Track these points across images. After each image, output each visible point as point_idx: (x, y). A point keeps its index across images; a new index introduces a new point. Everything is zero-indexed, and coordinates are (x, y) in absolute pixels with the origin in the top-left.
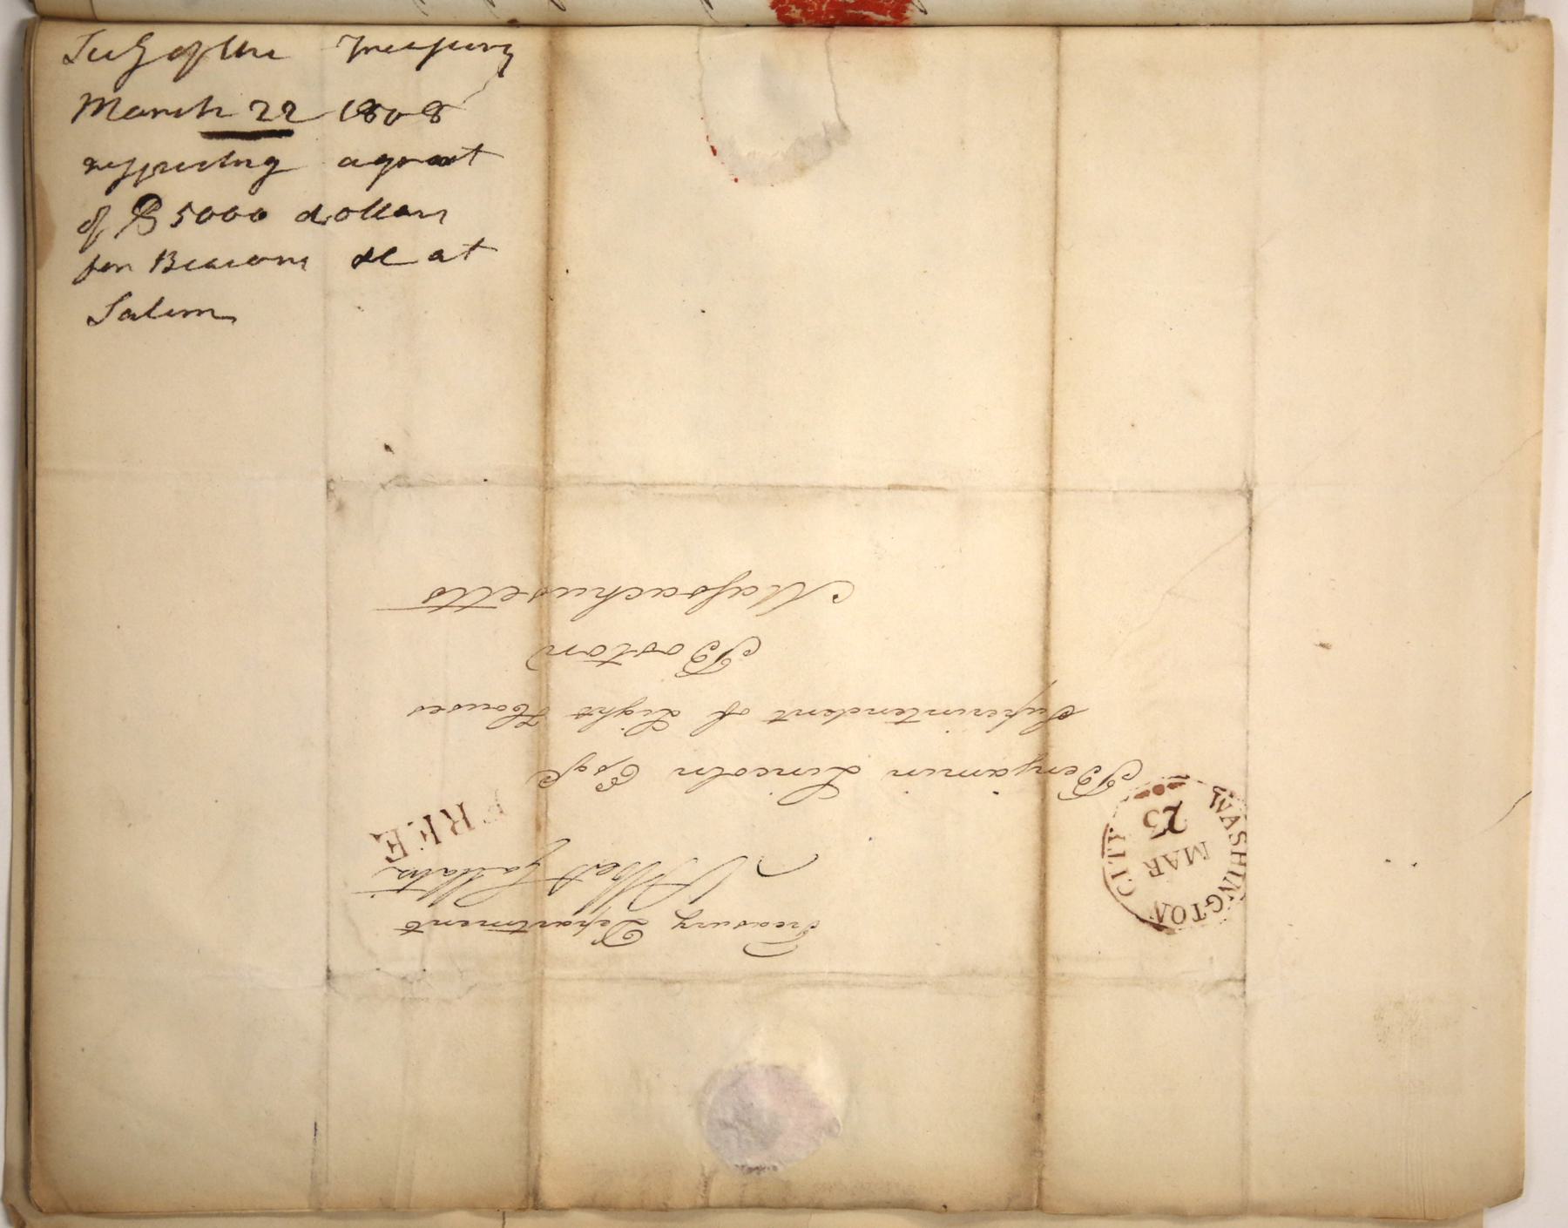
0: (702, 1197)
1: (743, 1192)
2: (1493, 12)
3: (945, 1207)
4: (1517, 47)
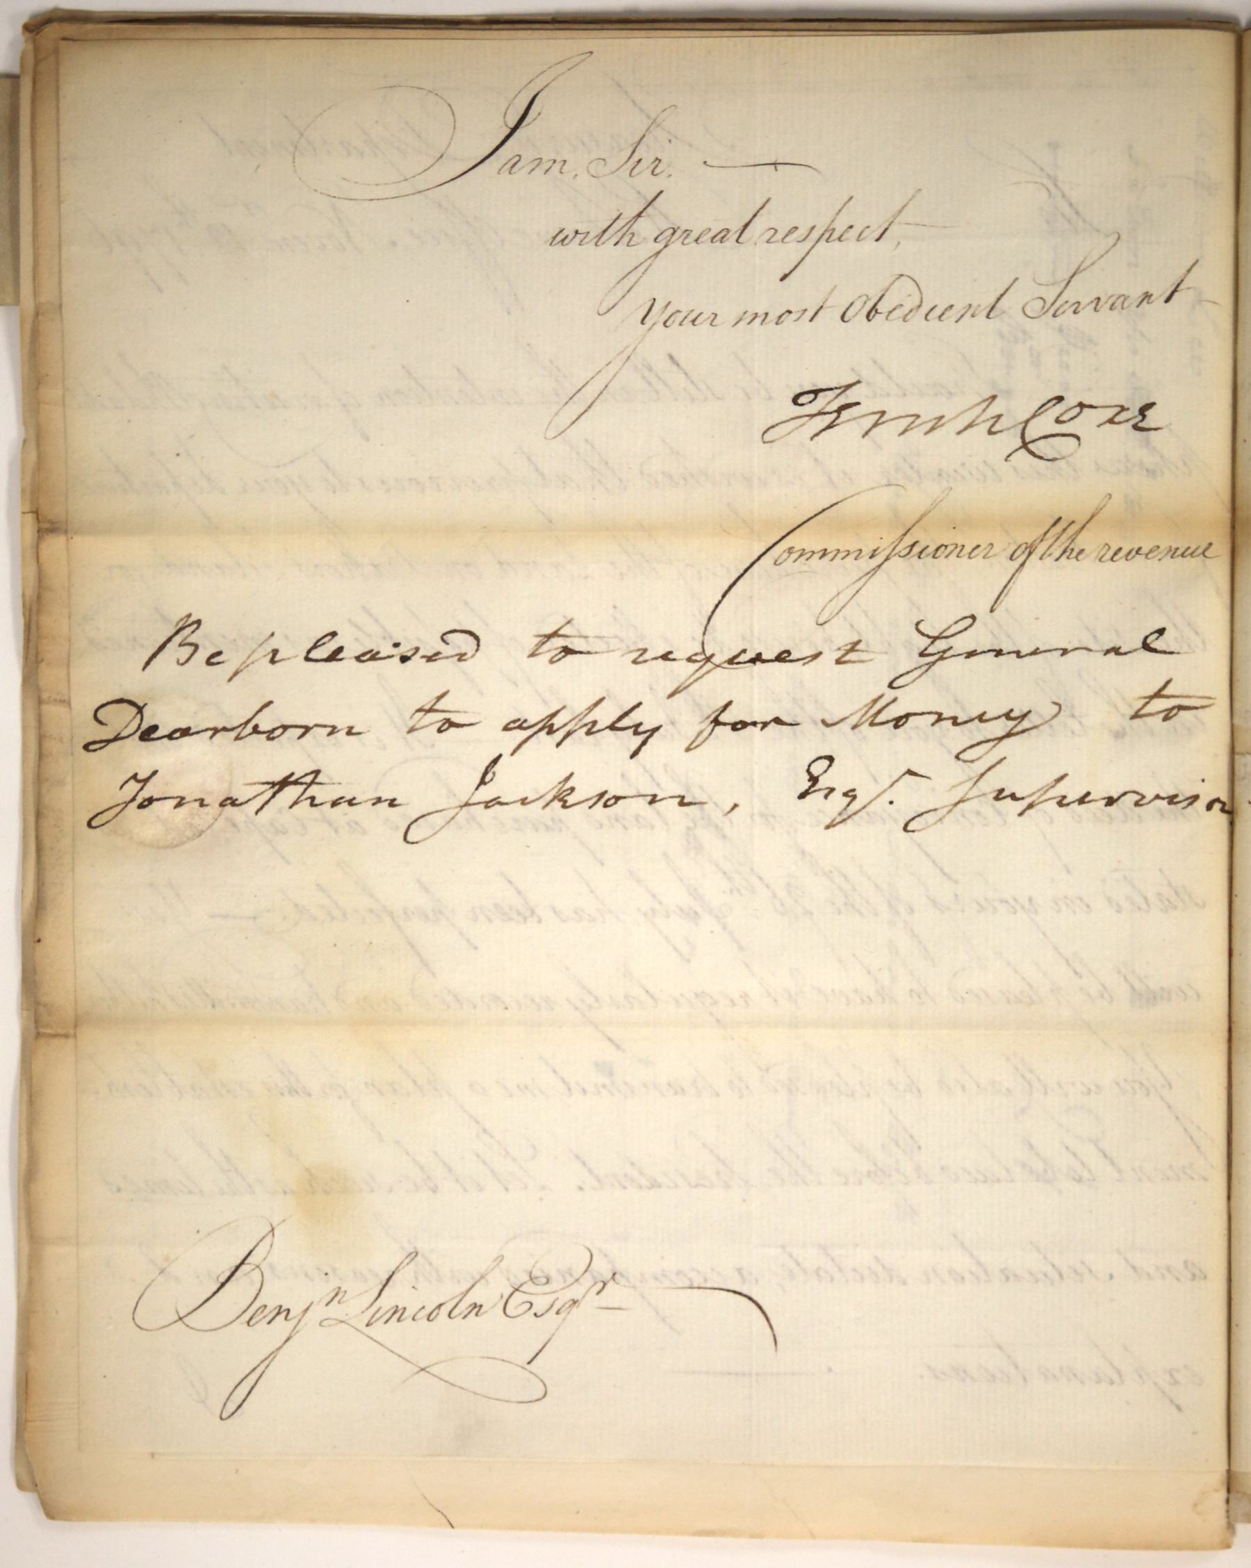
0: (50, 697)
1: (55, 739)
2: (1237, 1492)
3: (39, 941)
4: (1198, 1514)
